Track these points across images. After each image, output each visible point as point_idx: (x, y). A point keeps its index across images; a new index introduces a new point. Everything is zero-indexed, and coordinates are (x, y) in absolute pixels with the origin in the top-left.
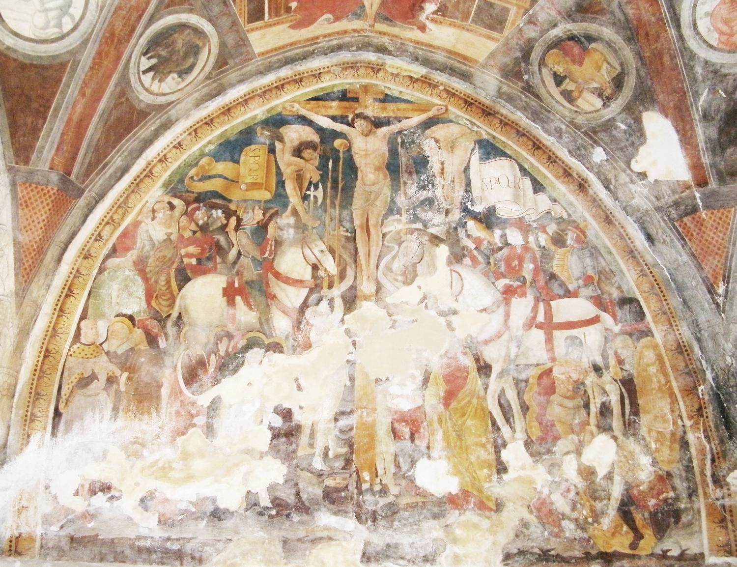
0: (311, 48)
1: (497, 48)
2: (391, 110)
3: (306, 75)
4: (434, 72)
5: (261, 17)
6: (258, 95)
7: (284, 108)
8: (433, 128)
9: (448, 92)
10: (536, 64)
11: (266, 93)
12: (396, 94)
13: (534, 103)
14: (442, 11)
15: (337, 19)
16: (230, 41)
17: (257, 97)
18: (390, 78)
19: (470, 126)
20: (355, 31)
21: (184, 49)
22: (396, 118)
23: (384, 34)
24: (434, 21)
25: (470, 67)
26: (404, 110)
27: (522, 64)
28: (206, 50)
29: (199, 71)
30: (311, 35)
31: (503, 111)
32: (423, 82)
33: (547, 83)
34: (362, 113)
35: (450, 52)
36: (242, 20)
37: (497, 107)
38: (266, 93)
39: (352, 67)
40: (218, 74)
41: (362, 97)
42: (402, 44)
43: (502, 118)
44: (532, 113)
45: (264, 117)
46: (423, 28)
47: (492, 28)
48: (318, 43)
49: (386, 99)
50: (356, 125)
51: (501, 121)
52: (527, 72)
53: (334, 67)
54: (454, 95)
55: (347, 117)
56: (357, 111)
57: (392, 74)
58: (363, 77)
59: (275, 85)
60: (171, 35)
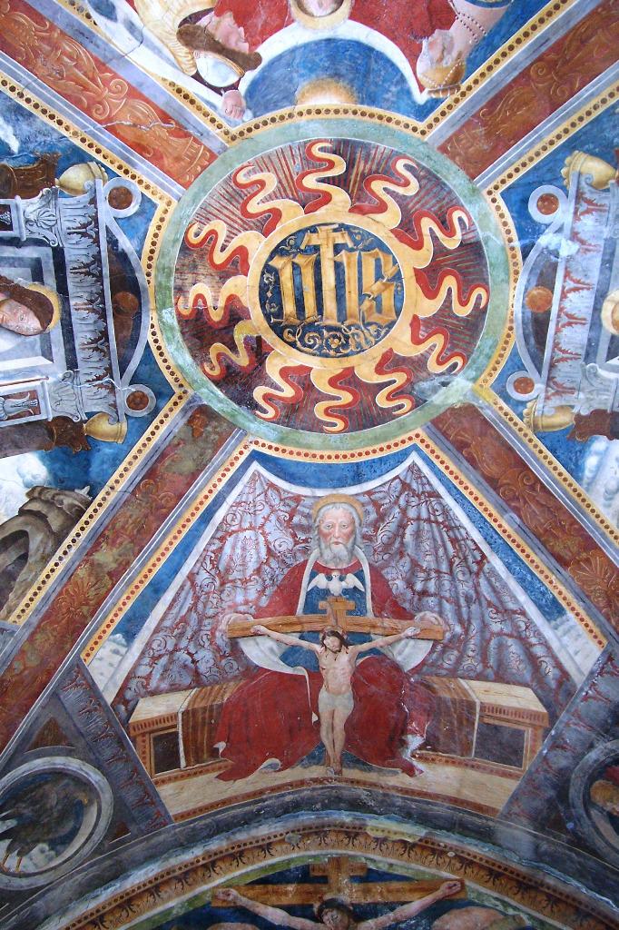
0: (254, 808)
1: (519, 788)
2: (378, 893)
3: (249, 846)
4: (438, 832)
5: (174, 763)
6: (175, 878)
7: (215, 897)
8: (446, 917)
9: (461, 859)
10: (579, 803)
11: (187, 875)
12: (384, 868)
13: (591, 862)
14: (431, 743)
15: (287, 765)
16: (131, 796)
17: (175, 881)
18: (373, 845)
19: (501, 908)
20: (315, 780)
21: (60, 807)
22: (386, 904)
23: (358, 782)
24: (422, 758)
25: (487, 819)
26: (398, 891)
27: (561, 808)
28: (94, 809)
29: (83, 840)
30: (250, 789)
31: (550, 881)
32: (423, 848)
33: (602, 830)
34: (333, 900)
35: (455, 800)
36: (147, 767)
37: (540, 876)
38: (187, 875)
39: (316, 833)
40: (114, 846)
41: (333, 875)
42: (385, 795)
43: (550, 892)
44: (594, 880)
45: (182, 912)
46: (410, 770)
47: (504, 760)
48: (264, 801)
49: (369, 877)
50: (325, 918)
51: (549, 896)
52: (570, 818)
53: (291, 834)
54: (471, 863)
55: (312, 906)
56: (327, 897)
57: (377, 840)
58: (333, 847)
59: (202, 862)
60: (40, 786)
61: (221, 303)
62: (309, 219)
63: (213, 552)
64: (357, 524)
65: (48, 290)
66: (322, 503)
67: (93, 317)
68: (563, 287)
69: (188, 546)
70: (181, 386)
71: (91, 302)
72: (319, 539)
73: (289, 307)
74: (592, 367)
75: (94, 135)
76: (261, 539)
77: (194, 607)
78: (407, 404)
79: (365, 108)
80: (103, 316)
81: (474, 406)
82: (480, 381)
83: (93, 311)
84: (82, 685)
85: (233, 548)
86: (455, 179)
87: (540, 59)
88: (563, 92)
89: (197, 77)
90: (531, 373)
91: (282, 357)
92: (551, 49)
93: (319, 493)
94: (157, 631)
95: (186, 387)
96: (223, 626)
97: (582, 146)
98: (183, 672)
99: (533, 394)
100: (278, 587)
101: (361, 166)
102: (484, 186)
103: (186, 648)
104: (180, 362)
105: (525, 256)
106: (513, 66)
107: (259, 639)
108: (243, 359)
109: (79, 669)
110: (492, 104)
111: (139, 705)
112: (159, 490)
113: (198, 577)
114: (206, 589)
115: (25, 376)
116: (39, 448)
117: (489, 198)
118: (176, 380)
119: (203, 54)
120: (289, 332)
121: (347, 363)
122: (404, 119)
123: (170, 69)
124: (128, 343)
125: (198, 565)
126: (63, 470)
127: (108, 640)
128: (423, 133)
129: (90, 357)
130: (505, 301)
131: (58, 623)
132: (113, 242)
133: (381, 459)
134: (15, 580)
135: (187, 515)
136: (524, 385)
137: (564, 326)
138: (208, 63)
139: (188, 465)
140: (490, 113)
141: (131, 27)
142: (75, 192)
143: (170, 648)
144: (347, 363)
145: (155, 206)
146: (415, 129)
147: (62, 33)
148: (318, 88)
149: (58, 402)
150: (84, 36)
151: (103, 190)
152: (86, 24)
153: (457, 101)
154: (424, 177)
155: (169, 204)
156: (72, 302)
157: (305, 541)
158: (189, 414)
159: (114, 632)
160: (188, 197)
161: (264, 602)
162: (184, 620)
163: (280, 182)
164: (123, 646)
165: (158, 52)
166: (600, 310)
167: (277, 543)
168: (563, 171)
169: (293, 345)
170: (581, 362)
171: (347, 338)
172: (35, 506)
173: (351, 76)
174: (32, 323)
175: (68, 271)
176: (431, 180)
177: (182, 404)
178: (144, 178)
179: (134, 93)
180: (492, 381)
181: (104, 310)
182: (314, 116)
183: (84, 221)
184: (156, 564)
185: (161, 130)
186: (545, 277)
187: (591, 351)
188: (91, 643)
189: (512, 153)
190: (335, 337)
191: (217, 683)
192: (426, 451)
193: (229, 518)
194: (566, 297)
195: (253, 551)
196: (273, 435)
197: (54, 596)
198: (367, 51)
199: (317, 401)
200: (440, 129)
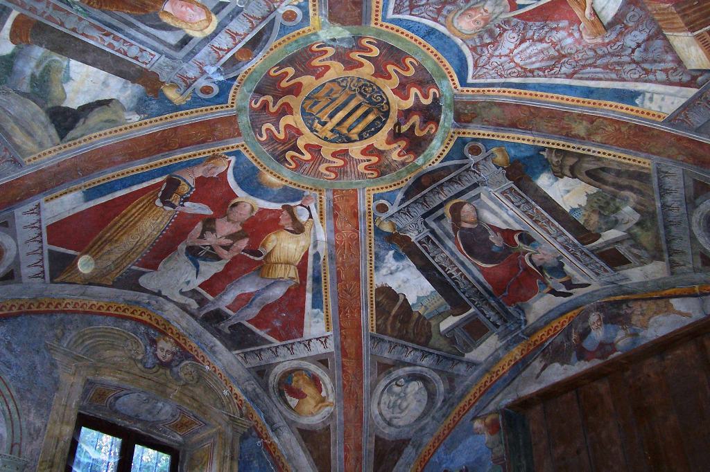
61: (395, 145)
62: (323, 144)
63: (544, 72)
64: (462, 11)
65: (447, 210)
66: (465, 37)
67: (445, 189)
68: (226, 53)
69: (549, 87)
70: (452, 137)
71: (438, 193)
72: (492, 21)
73: (371, 117)
74: (240, 4)
75: (365, 232)
76: (516, 51)
77: (593, 65)
78: (364, 42)
79: (259, 167)
80: (442, 184)
81: (329, 20)
82: (313, 31)
83: (442, 190)
84: (686, 115)
85: (534, 63)
86: (244, 120)
87: (170, 150)
88: (168, 134)
89: (311, 217)
90: (279, 20)
91: (398, 104)
92: (163, 151)
93: (459, 42)
94: (624, 80)
95: (451, 133)
96: (599, 40)
97: (173, 106)
98: (651, 50)
99: (289, 8)
100: (546, 21)
101: (281, 148)
102: (232, 110)
103: (629, 55)
104: (439, 144)
105: (236, 77)
106: (184, 152)
107: (598, 9)
108: (416, 119)
109: (671, 120)
110: (204, 142)
111: (694, 68)
112: (521, 117)
113: (567, 73)
114: (574, 64)
115: (496, 200)
116: (532, 181)
117: (234, 105)
118: (450, 140)
119: (301, 221)
120: (383, 109)
121: (373, 79)
122: (247, 155)
123: (317, 227)
124: (447, 170)
125: (559, 76)
126: (537, 168)
127: (643, 107)
128: (243, 146)
129: (466, 181)
130: (264, 63)
131: (639, 143)
132: (403, 201)
133: (409, 30)
134: (619, 171)
135: (528, 96)
136: (289, 16)
137: (241, 35)
138: (303, 217)
139: (496, 110)
140: (207, 139)
141: (315, 246)
142: (393, 225)
143: (634, 66)
144: (373, 79)
145: (374, 195)
146: (245, 148)
147: (336, 263)
148: (271, 185)
149: (500, 183)
150: (331, 257)
151: (384, 216)
152: (327, 259)
153: (218, 150)
154: (257, 128)
155: (369, 190)
156: (444, 199)
157: (499, 26)
158: (465, 124)
159: (636, 105)
160: (361, 186)
161: (564, 23)
162: (605, 67)
163: (319, 165)
164: (644, 97)
165: (315, 233)
166: (214, 32)
167: (513, 40)
168: (189, 99)
169: (388, 103)
170: (245, 11)
171: (360, 88)
172: (567, 172)
173: (255, 181)
174: (467, 208)
175: (430, 209)
176: (255, 126)
177: (462, 130)
178: (366, 205)
179: (336, 231)
180: (306, 28)
181: (438, 186)
182: (282, 177)
183: (403, 216)
184: (570, 100)
185: (341, 214)
186: (234, 62)
187: (235, 13)
188: (650, 117)
189: (210, 117)
190: (366, 92)
191: (653, 19)
192: (380, 14)
193: (515, 75)
194: (228, 48)
195: (529, 51)
196: (445, 83)
197: (621, 149)
198: (240, 184)
199: (406, 77)
200: (234, 144)
